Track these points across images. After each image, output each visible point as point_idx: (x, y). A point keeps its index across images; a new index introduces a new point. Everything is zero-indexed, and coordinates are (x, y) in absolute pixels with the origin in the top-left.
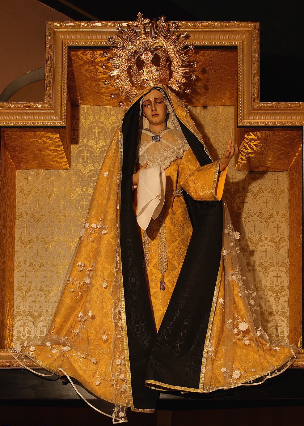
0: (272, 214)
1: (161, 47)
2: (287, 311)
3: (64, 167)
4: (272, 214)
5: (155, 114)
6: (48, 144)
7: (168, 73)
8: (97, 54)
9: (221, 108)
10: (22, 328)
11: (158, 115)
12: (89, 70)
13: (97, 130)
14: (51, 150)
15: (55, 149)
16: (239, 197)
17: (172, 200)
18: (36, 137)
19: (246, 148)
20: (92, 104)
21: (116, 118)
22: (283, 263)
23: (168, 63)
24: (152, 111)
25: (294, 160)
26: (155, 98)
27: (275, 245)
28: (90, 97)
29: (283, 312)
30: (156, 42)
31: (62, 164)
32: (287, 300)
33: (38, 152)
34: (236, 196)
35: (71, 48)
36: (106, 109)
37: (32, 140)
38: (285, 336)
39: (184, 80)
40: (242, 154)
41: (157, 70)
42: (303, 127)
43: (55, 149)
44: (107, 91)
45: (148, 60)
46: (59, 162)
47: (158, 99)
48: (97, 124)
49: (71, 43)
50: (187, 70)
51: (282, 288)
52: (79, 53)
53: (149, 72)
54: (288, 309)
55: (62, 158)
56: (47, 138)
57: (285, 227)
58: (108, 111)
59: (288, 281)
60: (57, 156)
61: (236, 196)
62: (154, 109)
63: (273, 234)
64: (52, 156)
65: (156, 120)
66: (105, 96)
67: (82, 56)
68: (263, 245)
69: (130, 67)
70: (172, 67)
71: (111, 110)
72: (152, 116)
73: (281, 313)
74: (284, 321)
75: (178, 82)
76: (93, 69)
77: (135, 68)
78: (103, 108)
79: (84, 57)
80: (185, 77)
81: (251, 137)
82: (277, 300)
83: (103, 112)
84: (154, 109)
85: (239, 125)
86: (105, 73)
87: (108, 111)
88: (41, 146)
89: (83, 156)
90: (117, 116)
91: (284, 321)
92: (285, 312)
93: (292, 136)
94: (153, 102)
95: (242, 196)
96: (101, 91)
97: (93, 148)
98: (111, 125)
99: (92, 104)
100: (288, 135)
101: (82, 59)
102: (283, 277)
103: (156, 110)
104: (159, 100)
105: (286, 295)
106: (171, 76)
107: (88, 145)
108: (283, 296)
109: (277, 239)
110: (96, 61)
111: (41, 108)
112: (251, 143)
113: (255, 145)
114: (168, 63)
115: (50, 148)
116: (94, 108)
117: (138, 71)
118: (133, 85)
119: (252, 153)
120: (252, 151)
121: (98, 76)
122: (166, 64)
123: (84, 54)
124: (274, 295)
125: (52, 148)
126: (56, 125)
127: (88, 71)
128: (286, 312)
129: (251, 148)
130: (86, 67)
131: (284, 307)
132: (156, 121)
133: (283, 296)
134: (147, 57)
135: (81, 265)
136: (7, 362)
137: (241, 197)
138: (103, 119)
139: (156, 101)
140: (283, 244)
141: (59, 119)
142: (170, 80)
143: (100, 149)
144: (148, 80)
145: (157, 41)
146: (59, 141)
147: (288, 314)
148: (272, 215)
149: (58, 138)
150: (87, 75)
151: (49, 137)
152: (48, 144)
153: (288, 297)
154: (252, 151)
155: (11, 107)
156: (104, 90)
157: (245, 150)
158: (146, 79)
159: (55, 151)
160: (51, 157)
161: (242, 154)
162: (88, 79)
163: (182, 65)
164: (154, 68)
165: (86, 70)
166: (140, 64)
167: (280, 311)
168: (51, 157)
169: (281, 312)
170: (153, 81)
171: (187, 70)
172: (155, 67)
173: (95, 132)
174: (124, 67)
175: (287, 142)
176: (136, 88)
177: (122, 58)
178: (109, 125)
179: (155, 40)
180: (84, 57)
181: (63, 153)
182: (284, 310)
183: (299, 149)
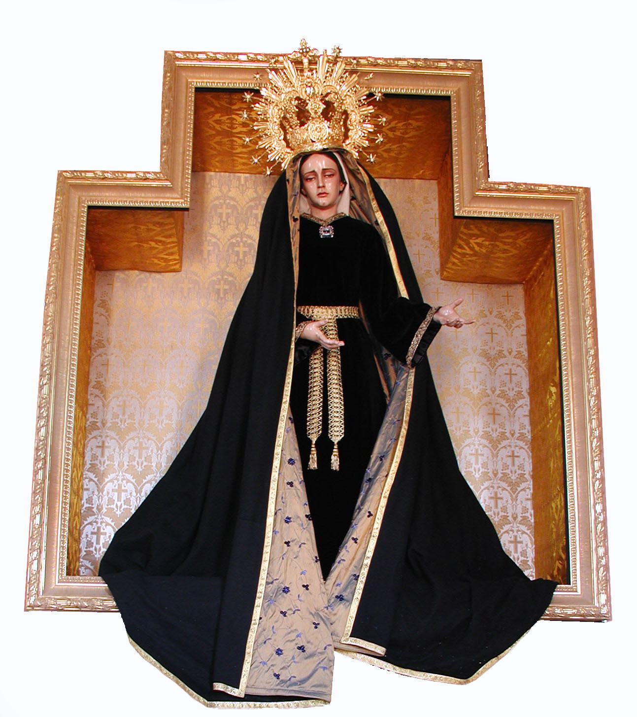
0: (501, 352)
2: (531, 515)
3: (173, 267)
4: (501, 352)
9: (418, 182)
13: (225, 211)
15: (163, 239)
16: (90, 523)
19: (460, 247)
20: (217, 170)
21: (254, 191)
22: (522, 434)
24: (319, 187)
25: (535, 268)
27: (508, 404)
28: (217, 159)
29: (524, 518)
31: (171, 263)
32: (529, 497)
34: (145, 479)
36: (239, 179)
38: (530, 559)
39: (366, 144)
40: (454, 256)
42: (180, 45)
43: (163, 239)
46: (166, 260)
48: (225, 201)
51: (522, 475)
54: (532, 512)
57: (523, 374)
58: (243, 182)
60: (164, 250)
61: (145, 479)
63: (504, 384)
66: (241, 158)
71: (246, 179)
72: (318, 195)
73: (521, 519)
74: (527, 534)
76: (228, 119)
77: (295, 121)
79: (216, 103)
81: (471, 232)
82: (514, 496)
83: (235, 183)
85: (456, 214)
87: (243, 182)
89: (238, 252)
90: (256, 189)
91: (527, 534)
92: (528, 518)
95: (97, 523)
96: (234, 151)
97: (218, 237)
99: (217, 170)
102: (505, 499)
103: (324, 187)
104: (330, 172)
106: (346, 137)
107: (212, 234)
108: (523, 490)
109: (511, 394)
110: (234, 131)
112: (471, 241)
113: (477, 244)
116: (220, 176)
119: (471, 255)
120: (471, 253)
121: (234, 128)
124: (509, 488)
128: (530, 517)
129: (469, 248)
130: (218, 139)
131: (525, 510)
133: (523, 490)
134: (315, 107)
136: (85, 600)
137: (95, 524)
138: (233, 193)
140: (521, 402)
142: (344, 142)
143: (229, 240)
144: (314, 142)
147: (533, 521)
148: (500, 354)
150: (217, 127)
153: (532, 491)
154: (471, 253)
156: (239, 150)
157: (459, 250)
160: (154, 252)
161: (454, 256)
162: (219, 133)
164: (326, 124)
166: (303, 116)
167: (519, 515)
173: (221, 214)
178: (244, 203)
182: (526, 515)
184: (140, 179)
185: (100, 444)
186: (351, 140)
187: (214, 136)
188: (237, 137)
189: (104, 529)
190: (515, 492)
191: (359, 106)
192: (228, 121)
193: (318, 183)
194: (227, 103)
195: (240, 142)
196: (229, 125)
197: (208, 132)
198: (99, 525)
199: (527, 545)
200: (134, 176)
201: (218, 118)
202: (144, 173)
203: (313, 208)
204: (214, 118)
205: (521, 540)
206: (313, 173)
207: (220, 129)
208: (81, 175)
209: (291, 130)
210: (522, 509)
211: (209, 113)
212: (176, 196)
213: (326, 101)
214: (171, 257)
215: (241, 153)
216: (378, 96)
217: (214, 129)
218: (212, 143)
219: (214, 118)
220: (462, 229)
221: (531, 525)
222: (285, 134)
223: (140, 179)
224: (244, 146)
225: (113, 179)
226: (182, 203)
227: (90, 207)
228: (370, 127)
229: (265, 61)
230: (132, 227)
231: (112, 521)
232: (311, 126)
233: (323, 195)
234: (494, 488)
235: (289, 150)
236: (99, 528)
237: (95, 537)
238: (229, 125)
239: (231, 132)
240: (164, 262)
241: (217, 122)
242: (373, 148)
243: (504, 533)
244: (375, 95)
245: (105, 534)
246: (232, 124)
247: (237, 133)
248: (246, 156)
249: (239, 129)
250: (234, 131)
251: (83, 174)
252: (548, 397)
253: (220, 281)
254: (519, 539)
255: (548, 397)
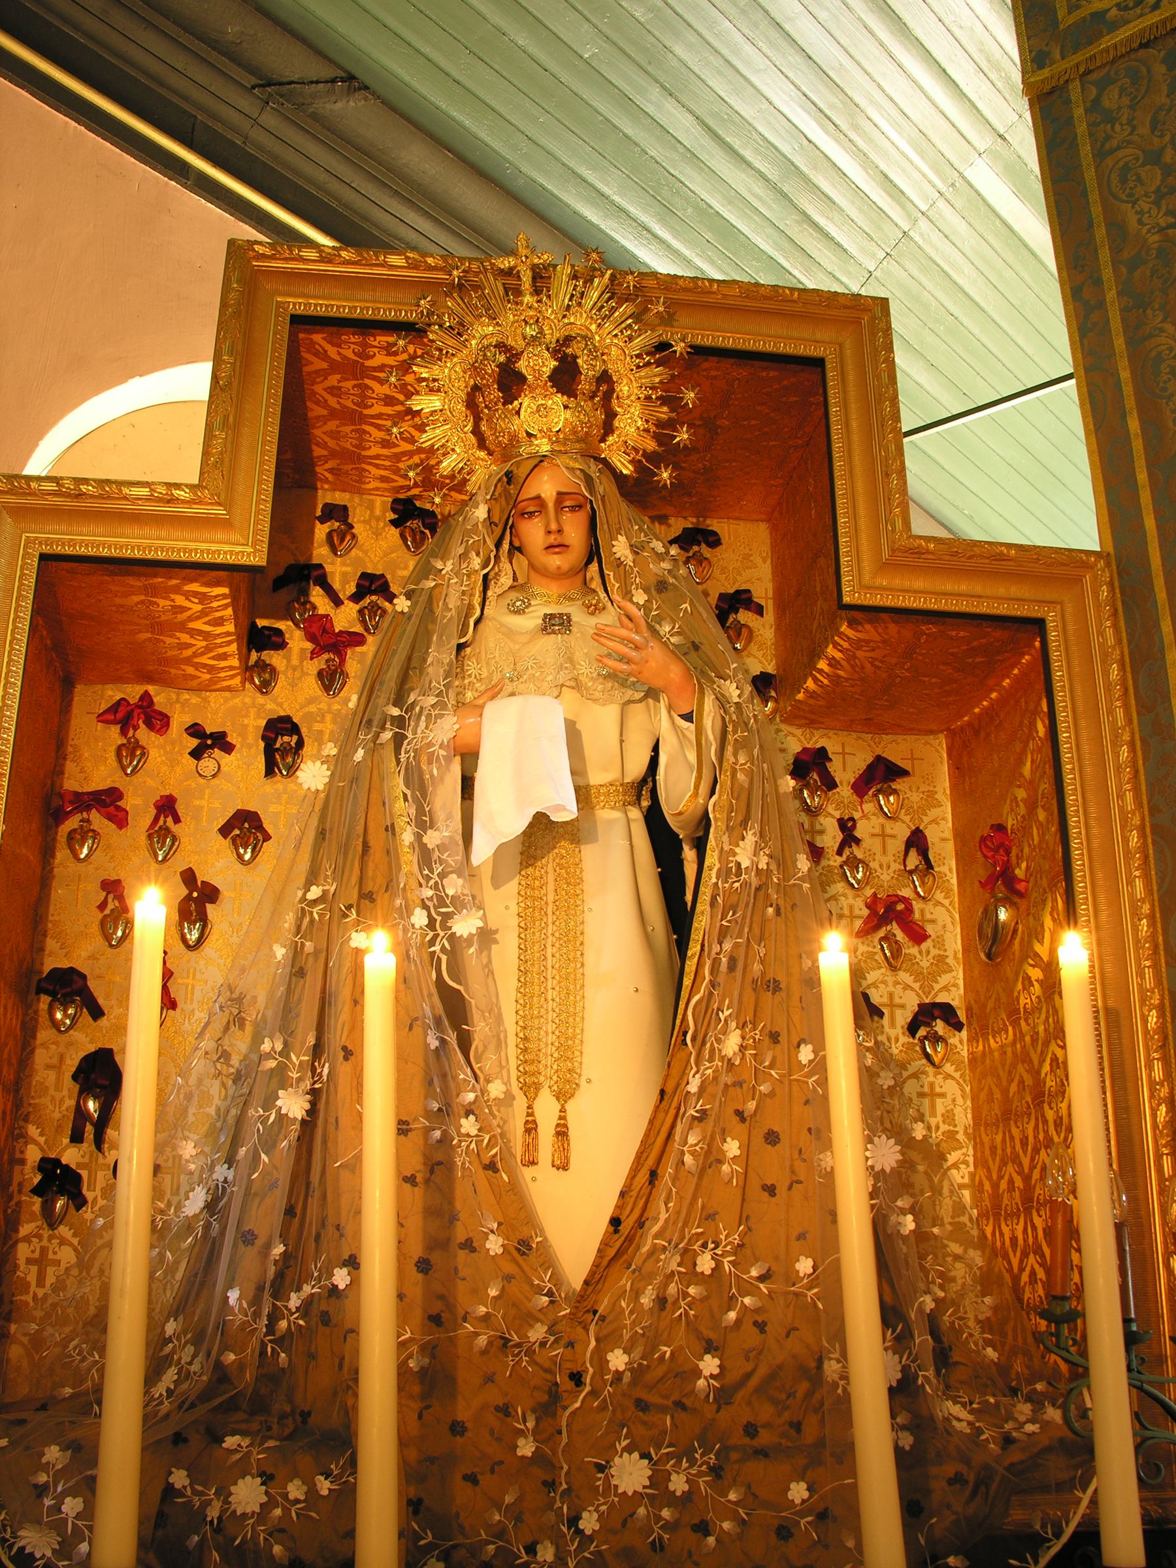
1: (585, 338)
2: (950, 870)
3: (225, 684)
5: (556, 543)
6: (189, 613)
7: (600, 416)
8: (376, 343)
10: (34, 1269)
11: (567, 546)
12: (340, 388)
14: (193, 633)
15: (208, 628)
17: (689, 897)
18: (154, 591)
23: (604, 388)
26: (559, 494)
30: (566, 321)
31: (222, 675)
33: (149, 635)
35: (299, 321)
37: (136, 599)
39: (651, 445)
41: (566, 407)
43: (208, 628)
44: (385, 452)
45: (538, 375)
46: (211, 669)
47: (567, 497)
49: (298, 304)
50: (664, 412)
52: (318, 338)
53: (538, 411)
55: (224, 657)
56: (188, 595)
59: (969, 1111)
60: (208, 649)
62: (554, 527)
64: (194, 649)
65: (555, 561)
66: (377, 466)
67: (328, 347)
68: (882, 982)
69: (476, 388)
70: (614, 401)
72: (547, 548)
75: (627, 449)
76: (353, 431)
77: (495, 394)
78: (361, 500)
79: (332, 352)
80: (657, 437)
84: (554, 527)
86: (389, 401)
88: (163, 618)
93: (997, 644)
94: (551, 505)
98: (386, 554)
100: (984, 641)
101: (324, 356)
102: (949, 1096)
103: (560, 531)
105: (966, 1163)
106: (608, 428)
110: (369, 363)
111: (188, 502)
114: (604, 388)
115: (191, 625)
117: (504, 405)
118: (482, 443)
121: (365, 449)
122: (598, 389)
123: (335, 341)
124: (916, 986)
125: (198, 625)
126: (231, 562)
127: (335, 391)
130: (333, 380)
132: (559, 568)
135: (273, 1048)
139: (561, 502)
141: (243, 542)
142: (603, 440)
145: (572, 320)
146: (226, 607)
149: (224, 596)
150: (333, 402)
151: (196, 594)
152: (189, 613)
155: (85, 494)
156: (375, 450)
158: (527, 433)
159: (206, 635)
160: (188, 653)
161: (836, 645)
162: (333, 414)
163: (648, 398)
165: (333, 387)
168: (188, 653)
169: (950, 1223)
170: (550, 439)
171: (664, 412)
172: (559, 399)
174: (460, 390)
175: (978, 660)
176: (490, 453)
177: (455, 360)
178: (380, 553)
179: (564, 316)
180: (332, 352)
181: (229, 643)
183: (1003, 680)
184: (160, 500)
185: (55, 1061)
186: (619, 436)
187: (325, 374)
188: (372, 424)
189: (55, 1253)
190: (929, 993)
191: (638, 367)
192: (354, 435)
193: (547, 525)
194: (354, 404)
195: (377, 434)
196: (356, 399)
197: (312, 410)
198: (45, 1243)
199: (954, 1100)
200: (145, 491)
201: (336, 384)
202: (169, 485)
203: (532, 573)
204: (327, 384)
205: (943, 1090)
206: (536, 502)
207: (338, 358)
208: (29, 486)
209: (486, 411)
210: (953, 1207)
211: (317, 372)
212: (234, 537)
213: (565, 355)
214: (223, 664)
215: (377, 457)
216: (679, 348)
217: (325, 404)
218: (319, 389)
219: (327, 384)
220: (844, 628)
221: (963, 1062)
222: (477, 420)
223: (160, 500)
224: (386, 444)
225: (101, 497)
226: (249, 555)
227: (43, 557)
228: (657, 374)
229: (442, 269)
230: (138, 603)
231: (75, 1235)
232: (526, 403)
233: (557, 550)
234: (887, 985)
235: (482, 454)
236: (44, 1250)
237: (34, 1269)
238: (356, 399)
239: (361, 413)
240: (209, 672)
241: (332, 390)
242: (666, 452)
243: (909, 1077)
244: (672, 346)
245: (58, 1263)
246: (364, 397)
247: (372, 417)
248: (387, 463)
249: (378, 409)
250: (369, 363)
251: (33, 485)
252: (1019, 986)
253: (323, 717)
254: (938, 1090)
255: (1019, 986)
